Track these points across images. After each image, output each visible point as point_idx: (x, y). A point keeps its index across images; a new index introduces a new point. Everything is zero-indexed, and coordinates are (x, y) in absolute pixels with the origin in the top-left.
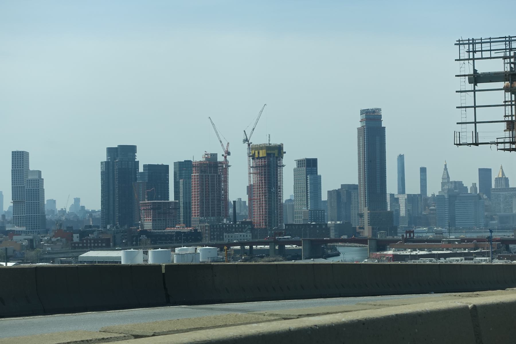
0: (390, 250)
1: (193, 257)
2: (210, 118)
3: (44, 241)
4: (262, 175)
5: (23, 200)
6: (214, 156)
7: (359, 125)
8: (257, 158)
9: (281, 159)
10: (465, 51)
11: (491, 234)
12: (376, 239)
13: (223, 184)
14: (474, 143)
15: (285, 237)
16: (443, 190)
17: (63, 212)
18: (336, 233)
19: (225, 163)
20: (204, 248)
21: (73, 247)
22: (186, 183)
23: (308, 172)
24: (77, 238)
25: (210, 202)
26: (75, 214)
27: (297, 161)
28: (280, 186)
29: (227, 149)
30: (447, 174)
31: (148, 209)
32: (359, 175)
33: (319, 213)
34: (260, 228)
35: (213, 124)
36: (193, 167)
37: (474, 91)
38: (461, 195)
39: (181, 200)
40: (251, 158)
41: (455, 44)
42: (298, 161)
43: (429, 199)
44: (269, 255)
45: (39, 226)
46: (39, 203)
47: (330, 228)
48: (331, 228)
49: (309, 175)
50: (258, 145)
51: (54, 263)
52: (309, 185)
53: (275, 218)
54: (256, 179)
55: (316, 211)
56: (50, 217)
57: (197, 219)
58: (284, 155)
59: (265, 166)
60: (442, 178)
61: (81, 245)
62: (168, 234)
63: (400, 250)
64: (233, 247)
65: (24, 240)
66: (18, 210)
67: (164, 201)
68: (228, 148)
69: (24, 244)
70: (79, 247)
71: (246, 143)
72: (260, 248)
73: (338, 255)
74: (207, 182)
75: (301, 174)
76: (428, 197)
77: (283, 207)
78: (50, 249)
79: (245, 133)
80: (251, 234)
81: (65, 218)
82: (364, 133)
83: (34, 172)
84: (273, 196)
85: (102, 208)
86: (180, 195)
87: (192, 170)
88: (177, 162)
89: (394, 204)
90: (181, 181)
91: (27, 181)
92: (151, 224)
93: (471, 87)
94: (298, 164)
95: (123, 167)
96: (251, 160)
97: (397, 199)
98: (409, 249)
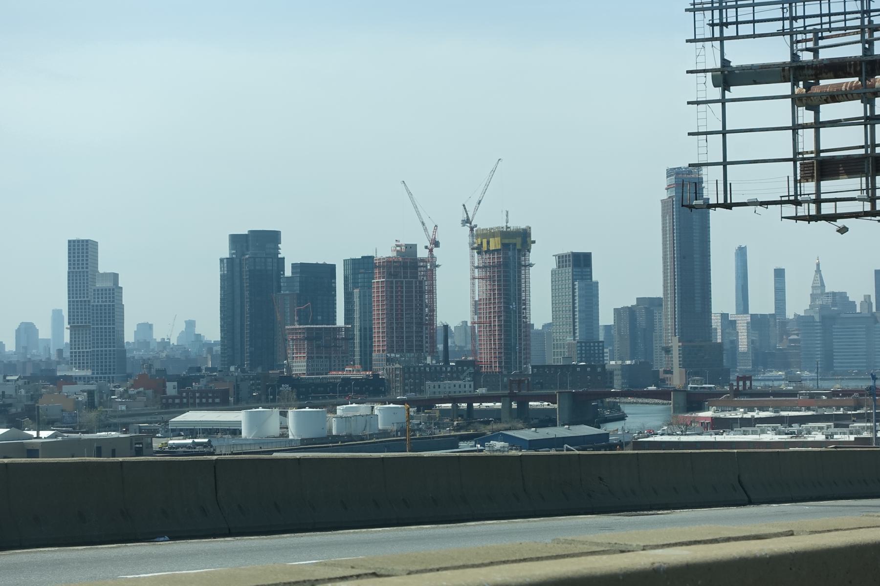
0: (709, 410)
1: (366, 421)
2: (404, 183)
3: (117, 394)
4: (494, 281)
5: (88, 324)
6: (412, 248)
7: (665, 195)
8: (486, 252)
9: (528, 253)
10: (705, 24)
11: (875, 382)
12: (685, 391)
13: (426, 296)
14: (720, 204)
15: (704, 386)
16: (812, 307)
17: (164, 344)
18: (623, 381)
19: (431, 261)
20: (385, 406)
21: (164, 404)
22: (365, 296)
23: (576, 275)
24: (174, 388)
25: (404, 327)
26: (185, 348)
27: (557, 257)
28: (525, 300)
29: (434, 236)
30: (820, 280)
31: (300, 340)
32: (665, 281)
33: (594, 346)
34: (490, 372)
35: (410, 193)
36: (376, 267)
37: (723, 101)
38: (843, 315)
39: (357, 324)
40: (475, 251)
41: (687, 10)
42: (559, 257)
43: (788, 322)
44: (500, 419)
45: (114, 369)
46: (114, 328)
47: (613, 371)
48: (615, 373)
49: (578, 280)
50: (487, 229)
51: (128, 432)
52: (577, 298)
53: (516, 355)
54: (484, 288)
55: (590, 343)
56: (141, 353)
57: (382, 357)
58: (533, 245)
59: (499, 266)
60: (812, 287)
61: (177, 401)
62: (330, 382)
63: (725, 409)
64: (440, 405)
65: (81, 393)
66: (79, 341)
67: (326, 326)
68: (436, 232)
69: (80, 399)
70: (174, 405)
71: (468, 226)
72: (486, 406)
73: (622, 418)
74: (399, 293)
75: (557, 279)
76: (788, 319)
77: (529, 336)
78: (124, 408)
79: (465, 208)
80: (472, 383)
81: (166, 355)
82: (673, 208)
83: (105, 275)
84: (512, 317)
85: (221, 337)
86: (355, 316)
87: (373, 273)
88: (348, 260)
89: (727, 331)
90: (356, 291)
91: (94, 290)
92: (305, 364)
93: (716, 93)
94: (559, 261)
95: (258, 268)
96: (476, 254)
97: (734, 323)
98: (742, 408)
